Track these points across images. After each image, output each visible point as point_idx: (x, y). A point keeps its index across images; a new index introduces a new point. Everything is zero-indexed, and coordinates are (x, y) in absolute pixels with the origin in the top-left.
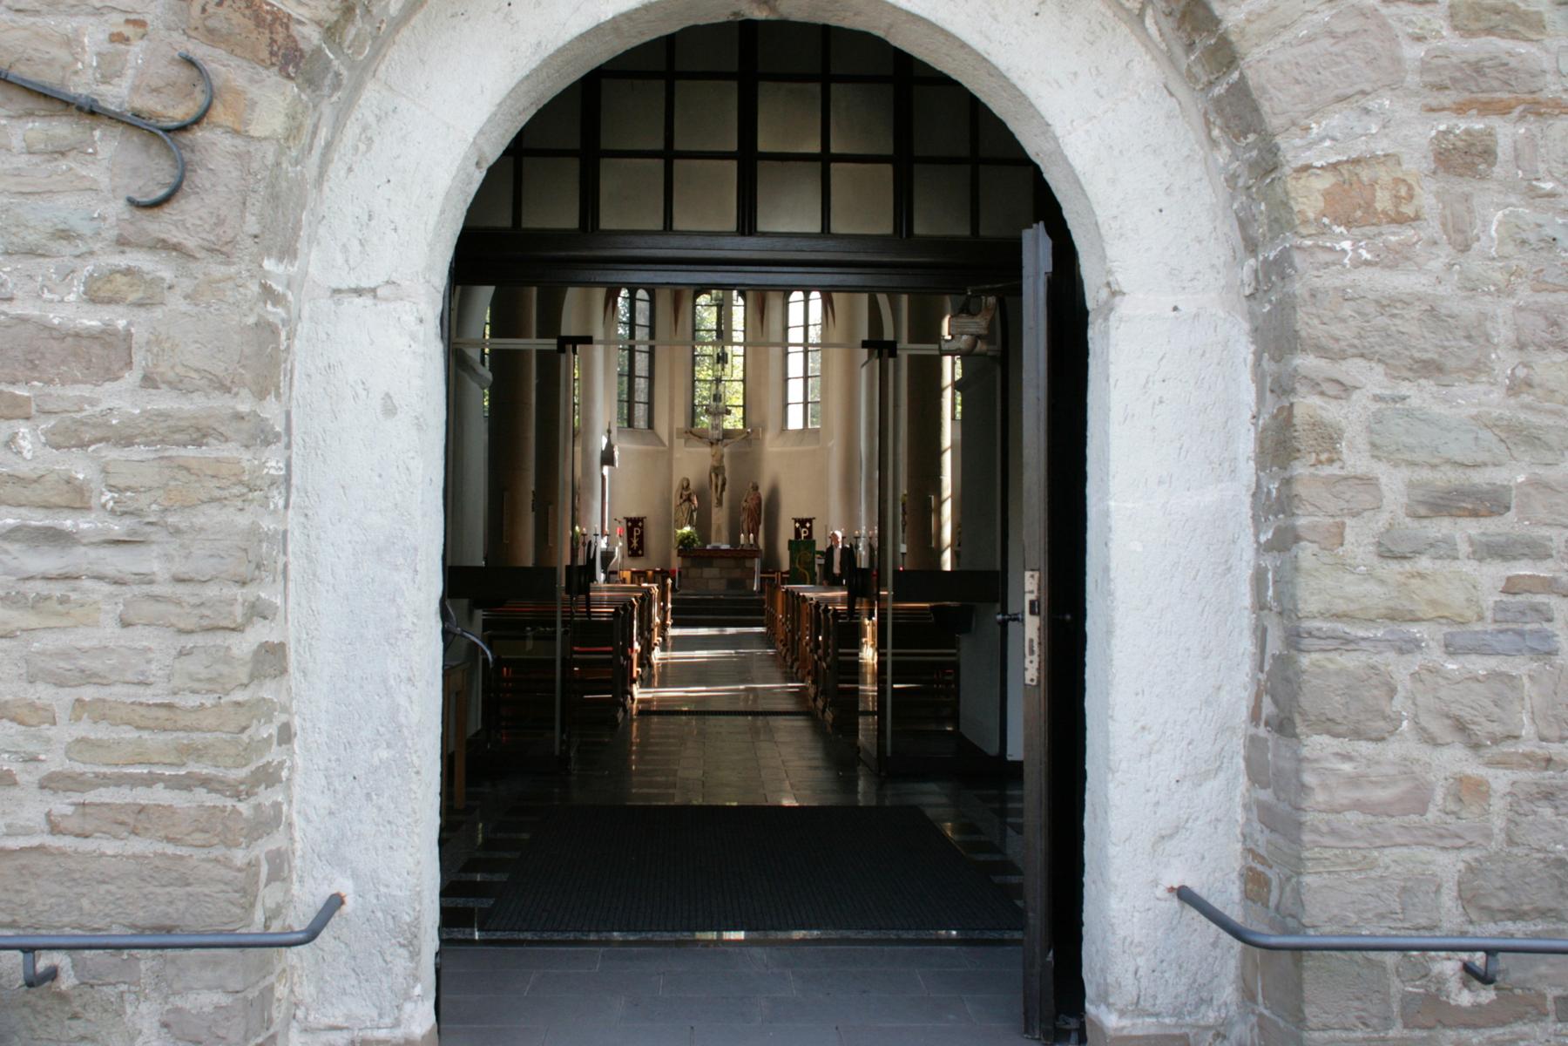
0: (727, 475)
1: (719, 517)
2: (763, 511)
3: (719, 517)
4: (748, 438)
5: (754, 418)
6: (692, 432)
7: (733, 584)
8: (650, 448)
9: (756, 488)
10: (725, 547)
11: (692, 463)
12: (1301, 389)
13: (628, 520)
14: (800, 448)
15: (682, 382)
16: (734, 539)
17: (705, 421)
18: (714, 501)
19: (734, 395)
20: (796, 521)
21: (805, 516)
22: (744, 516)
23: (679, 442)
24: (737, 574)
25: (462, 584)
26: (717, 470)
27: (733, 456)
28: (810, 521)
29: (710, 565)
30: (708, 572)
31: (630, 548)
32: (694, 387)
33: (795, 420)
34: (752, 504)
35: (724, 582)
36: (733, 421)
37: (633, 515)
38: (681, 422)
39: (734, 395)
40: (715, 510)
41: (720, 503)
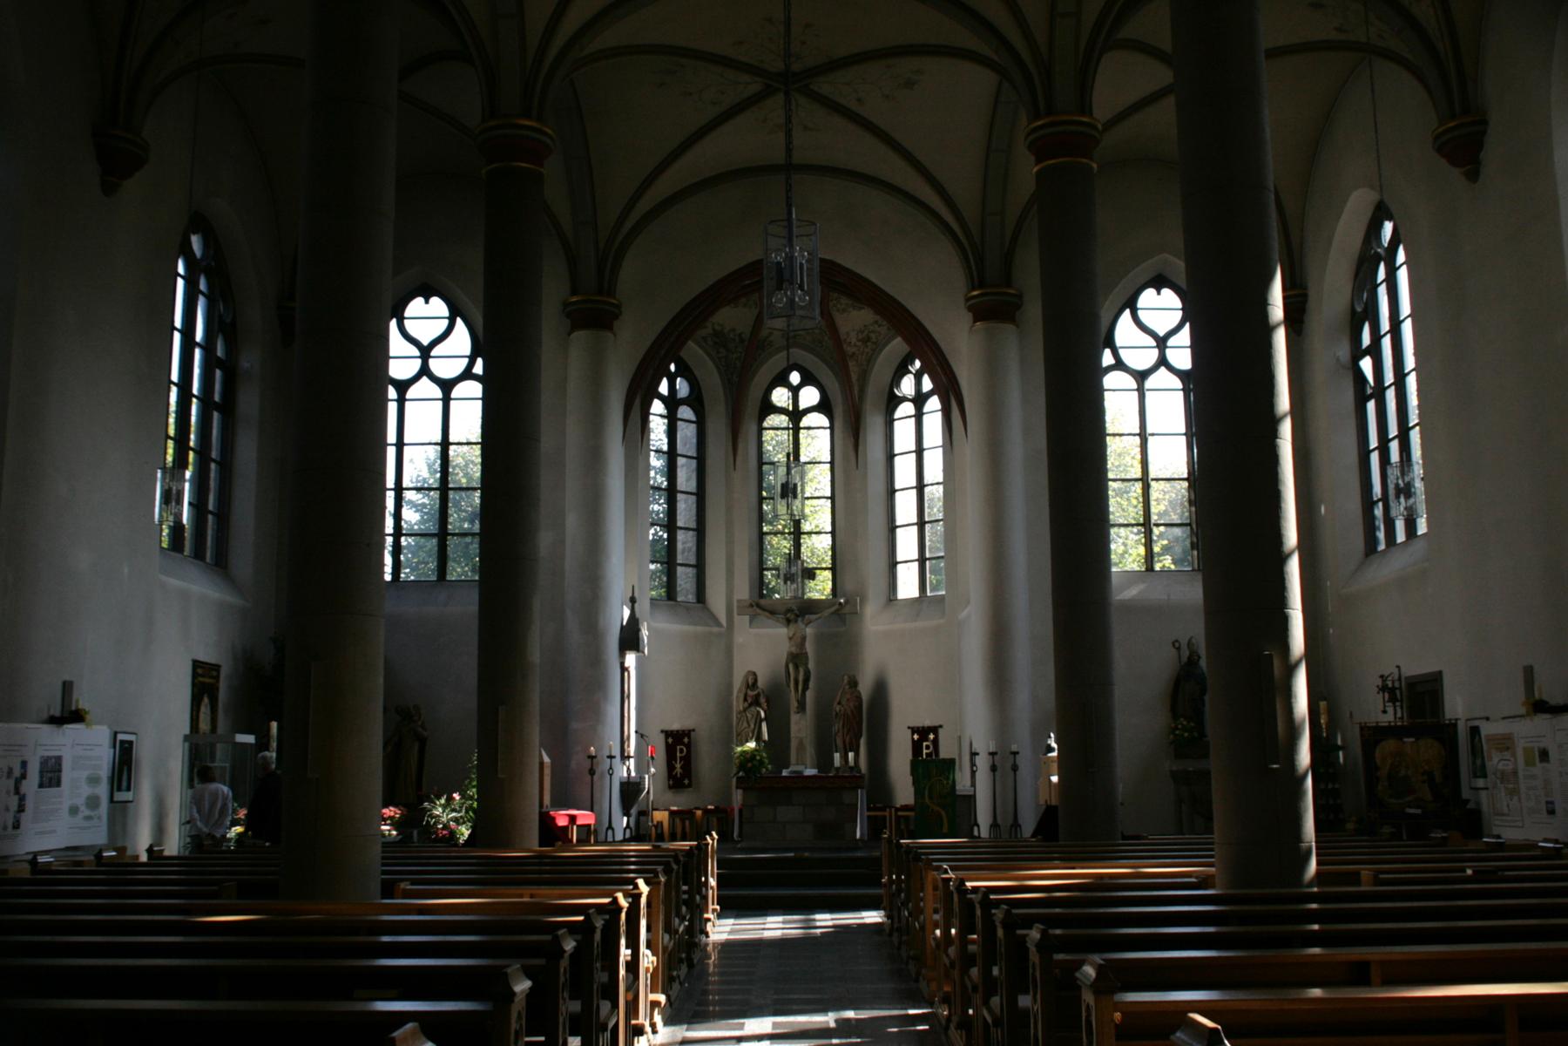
0: (811, 665)
1: (801, 727)
2: (864, 716)
3: (801, 727)
6: (760, 604)
8: (699, 629)
9: (854, 684)
10: (810, 772)
11: (761, 649)
14: (919, 624)
15: (744, 536)
18: (794, 704)
20: (914, 730)
21: (927, 723)
22: (837, 726)
23: (742, 621)
27: (820, 639)
28: (935, 729)
33: (908, 585)
36: (821, 588)
38: (743, 592)
40: (794, 718)
41: (802, 707)
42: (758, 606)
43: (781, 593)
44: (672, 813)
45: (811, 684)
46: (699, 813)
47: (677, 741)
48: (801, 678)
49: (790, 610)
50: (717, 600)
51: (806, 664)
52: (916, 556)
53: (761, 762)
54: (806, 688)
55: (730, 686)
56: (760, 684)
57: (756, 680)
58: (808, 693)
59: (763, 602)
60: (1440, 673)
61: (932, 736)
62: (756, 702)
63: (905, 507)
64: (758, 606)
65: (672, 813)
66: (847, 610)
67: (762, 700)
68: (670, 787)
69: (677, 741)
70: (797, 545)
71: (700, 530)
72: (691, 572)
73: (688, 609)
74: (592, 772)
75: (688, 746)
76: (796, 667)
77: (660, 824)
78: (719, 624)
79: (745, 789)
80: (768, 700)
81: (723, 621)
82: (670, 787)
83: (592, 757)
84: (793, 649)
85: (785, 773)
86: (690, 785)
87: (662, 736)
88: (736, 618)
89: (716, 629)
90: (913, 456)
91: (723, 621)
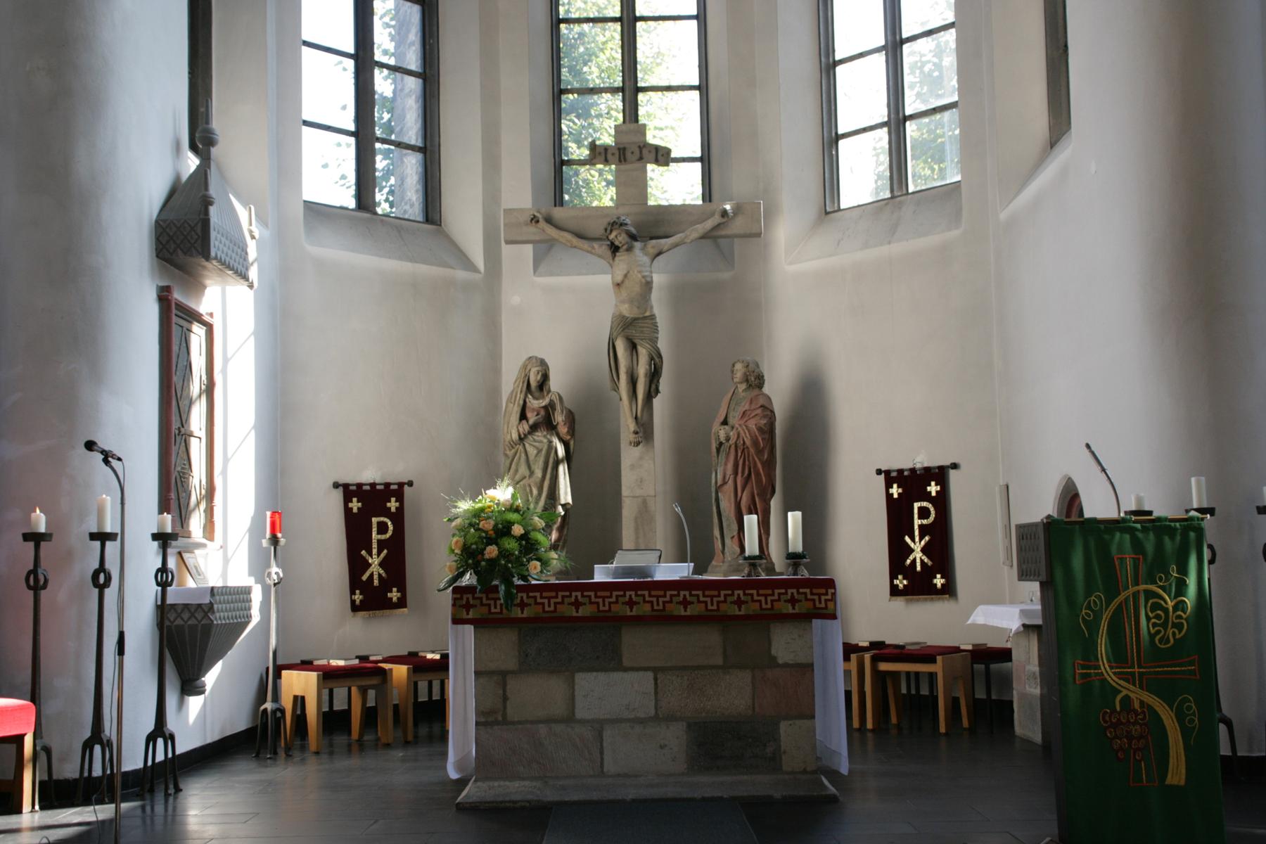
0: (663, 345)
1: (644, 476)
2: (782, 454)
3: (644, 476)
4: (724, 233)
5: (738, 184)
6: (554, 223)
7: (716, 742)
8: (423, 269)
9: (755, 381)
10: (671, 571)
11: (558, 317)
12: (189, 585)
13: (349, 491)
14: (897, 248)
15: (521, 86)
16: (695, 541)
17: (599, 190)
18: (628, 425)
19: (674, 122)
20: (890, 478)
21: (923, 460)
22: (722, 470)
23: (518, 257)
24: (733, 695)
25: (158, 607)
26: (632, 329)
27: (681, 295)
28: (940, 474)
29: (609, 659)
30: (604, 693)
31: (355, 582)
32: (555, 35)
33: (862, 173)
34: (745, 429)
35: (675, 737)
36: (675, 186)
37: (369, 475)
38: (520, 193)
39: (674, 122)
40: (629, 455)
41: (644, 431)
42: (549, 220)
43: (599, 190)
44: (329, 676)
45: (664, 383)
46: (400, 672)
47: (373, 511)
48: (642, 370)
49: (616, 224)
50: (466, 216)
51: (654, 341)
52: (882, 114)
53: (528, 545)
54: (652, 392)
55: (495, 391)
56: (555, 384)
57: (545, 377)
58: (657, 402)
59: (558, 213)
60: (1020, 579)
61: (933, 489)
62: (547, 423)
63: (861, 94)
64: (549, 220)
65: (329, 676)
66: (737, 226)
67: (559, 418)
68: (355, 608)
69: (373, 511)
70: (631, 111)
71: (429, 76)
72: (412, 164)
73: (399, 229)
74: (36, 582)
75: (398, 517)
76: (633, 347)
77: (300, 701)
78: (468, 265)
79: (478, 623)
80: (555, 418)
81: (479, 260)
82: (355, 608)
83: (36, 538)
84: (626, 310)
85: (601, 574)
86: (402, 603)
87: (338, 495)
88: (506, 250)
89: (461, 274)
90: (880, 59)
91: (479, 260)
